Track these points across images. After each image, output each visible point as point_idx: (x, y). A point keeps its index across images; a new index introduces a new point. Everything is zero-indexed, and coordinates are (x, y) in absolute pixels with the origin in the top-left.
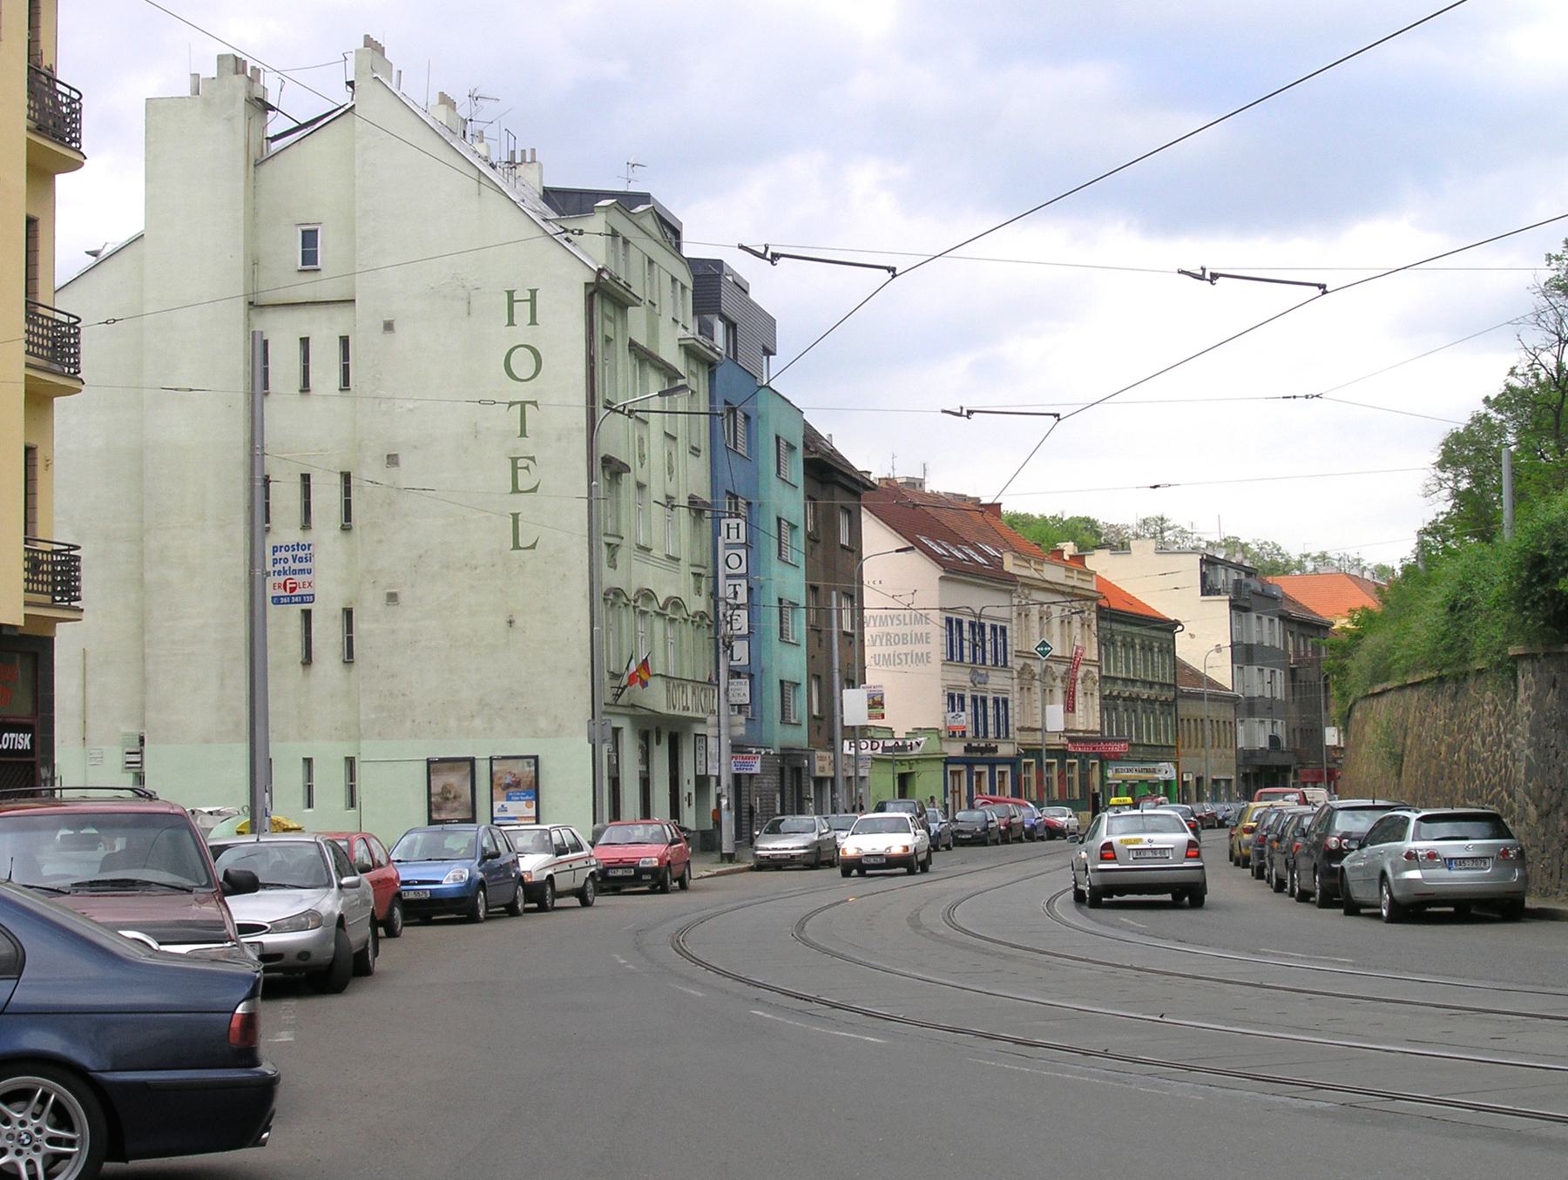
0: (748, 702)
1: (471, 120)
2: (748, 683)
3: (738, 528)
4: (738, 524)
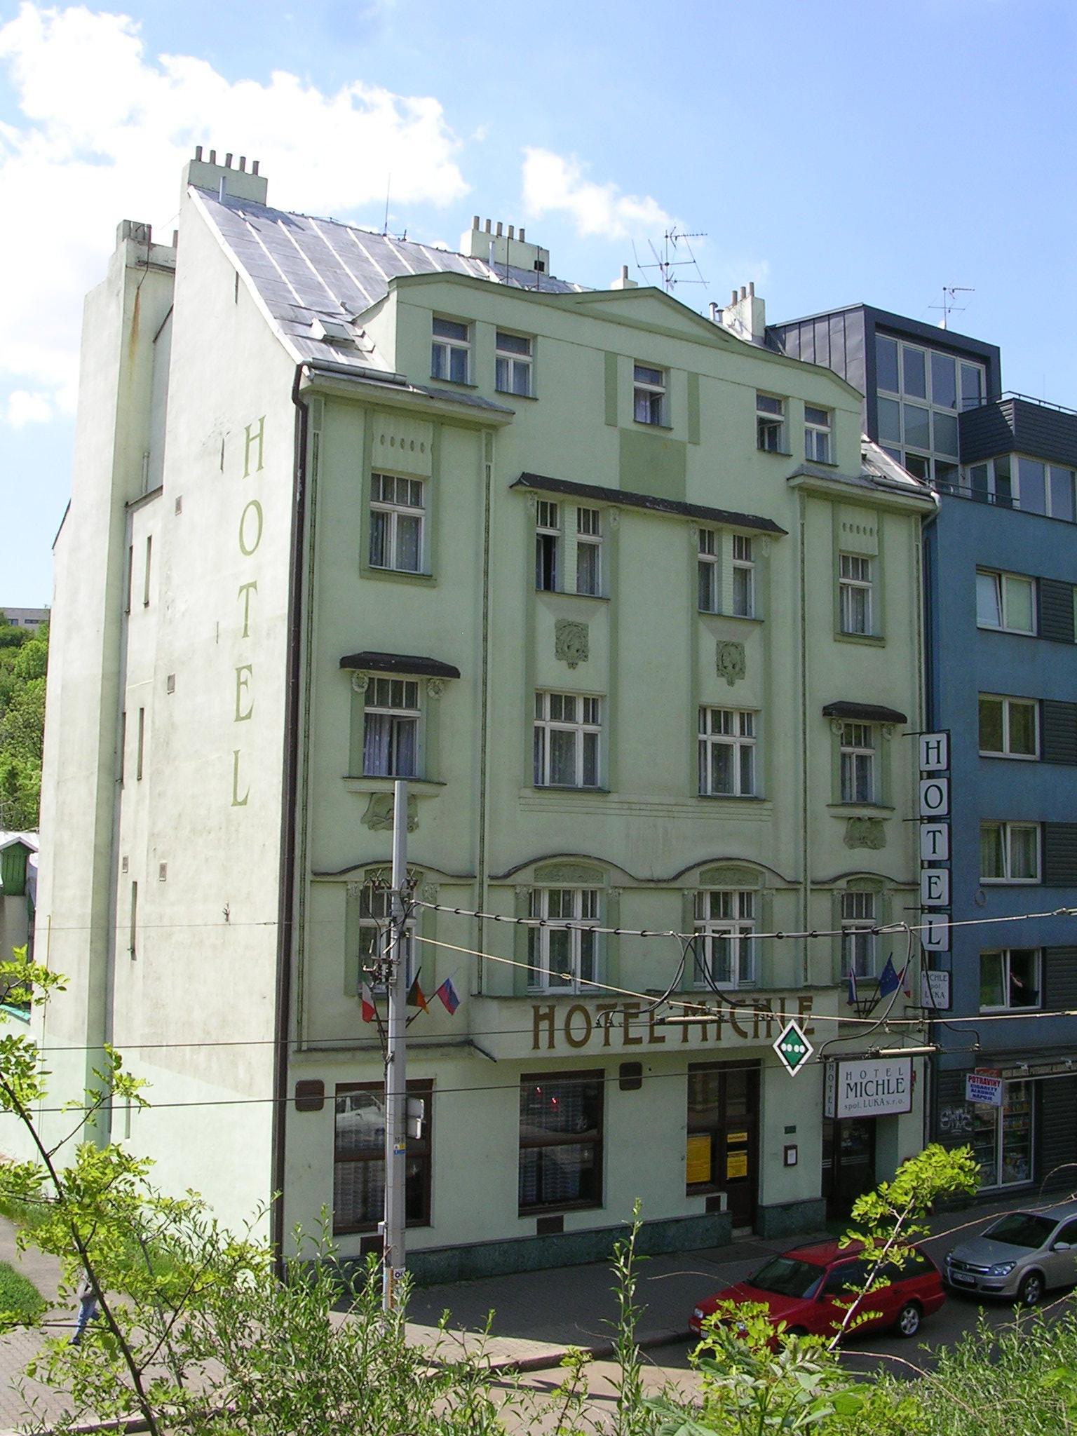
0: (946, 1006)
1: (667, 264)
2: (947, 978)
3: (938, 748)
4: (939, 742)
